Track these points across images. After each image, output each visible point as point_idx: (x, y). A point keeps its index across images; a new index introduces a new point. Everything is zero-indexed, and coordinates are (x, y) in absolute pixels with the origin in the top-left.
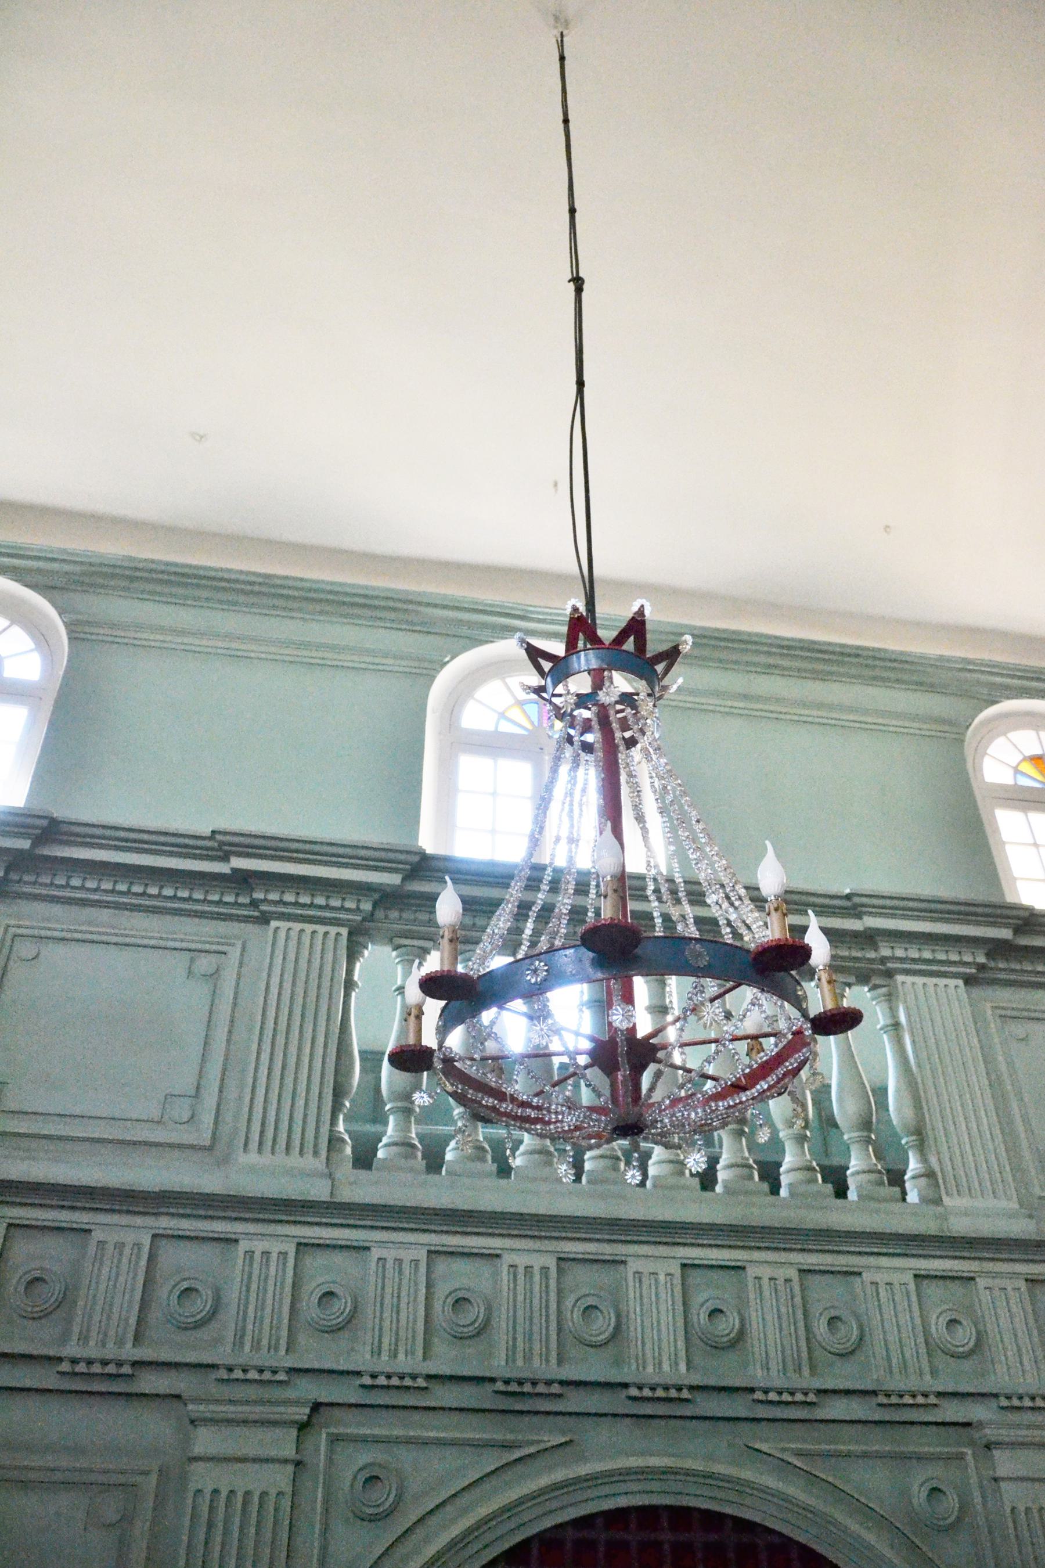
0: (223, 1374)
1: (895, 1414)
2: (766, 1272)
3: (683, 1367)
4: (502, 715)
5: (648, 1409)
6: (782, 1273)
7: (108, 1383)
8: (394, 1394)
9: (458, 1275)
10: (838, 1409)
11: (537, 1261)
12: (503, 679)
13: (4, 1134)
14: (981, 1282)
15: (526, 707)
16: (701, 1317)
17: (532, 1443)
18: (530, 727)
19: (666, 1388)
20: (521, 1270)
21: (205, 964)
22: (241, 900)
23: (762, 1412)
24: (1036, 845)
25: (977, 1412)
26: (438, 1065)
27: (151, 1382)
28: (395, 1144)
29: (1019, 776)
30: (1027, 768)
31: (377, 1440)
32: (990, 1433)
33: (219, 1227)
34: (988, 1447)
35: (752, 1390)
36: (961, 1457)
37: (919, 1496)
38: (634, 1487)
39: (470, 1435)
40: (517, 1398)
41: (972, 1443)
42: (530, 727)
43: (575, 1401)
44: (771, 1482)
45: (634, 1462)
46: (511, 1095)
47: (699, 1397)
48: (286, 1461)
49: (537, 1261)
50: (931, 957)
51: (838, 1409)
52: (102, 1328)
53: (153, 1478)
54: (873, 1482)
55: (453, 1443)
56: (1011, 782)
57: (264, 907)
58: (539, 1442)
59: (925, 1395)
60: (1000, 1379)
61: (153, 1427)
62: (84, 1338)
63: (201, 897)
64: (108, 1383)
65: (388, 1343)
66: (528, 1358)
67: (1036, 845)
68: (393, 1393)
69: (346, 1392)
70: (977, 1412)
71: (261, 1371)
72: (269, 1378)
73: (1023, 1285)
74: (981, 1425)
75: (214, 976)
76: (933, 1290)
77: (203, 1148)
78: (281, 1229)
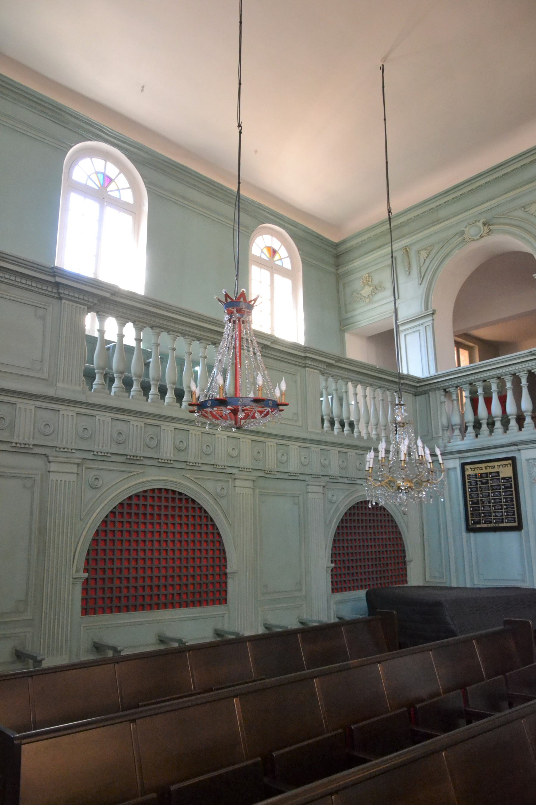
0: (58, 449)
1: (217, 470)
2: (194, 432)
3: (172, 456)
4: (89, 177)
5: (162, 465)
6: (198, 433)
7: (23, 450)
8: (102, 457)
9: (120, 426)
10: (205, 468)
11: (140, 424)
12: (91, 159)
13: (1, 371)
14: (241, 440)
15: (98, 175)
16: (177, 442)
17: (134, 472)
18: (99, 186)
19: (134, 456)
20: (135, 426)
21: (41, 312)
22: (54, 291)
23: (188, 467)
24: (261, 282)
25: (234, 471)
26: (186, 398)
27: (37, 450)
28: (99, 384)
29: (262, 254)
30: (265, 251)
31: (98, 469)
32: (237, 476)
33: (54, 406)
34: (235, 479)
35: (187, 462)
36: (228, 481)
37: (219, 489)
38: (158, 484)
39: (122, 469)
40: (132, 460)
41: (231, 478)
42: (99, 186)
43: (146, 462)
44: (189, 484)
45: (158, 478)
46: (227, 420)
47: (228, 468)
48: (75, 473)
49: (140, 424)
50: (122, 176)
51: (205, 468)
52: (24, 432)
53: (40, 476)
54: (210, 486)
55: (117, 471)
56: (259, 255)
57: (62, 295)
58: (134, 472)
59: (107, 453)
60: (241, 464)
61: (36, 463)
62: (18, 436)
63: (40, 287)
64: (23, 450)
65: (103, 444)
66: (136, 450)
67: (261, 282)
68: (66, 454)
69: (90, 456)
70: (234, 471)
71: (68, 449)
72: (70, 451)
73: (250, 441)
74: (235, 474)
75: (43, 318)
76: (231, 440)
77: (45, 379)
78: (72, 408)
